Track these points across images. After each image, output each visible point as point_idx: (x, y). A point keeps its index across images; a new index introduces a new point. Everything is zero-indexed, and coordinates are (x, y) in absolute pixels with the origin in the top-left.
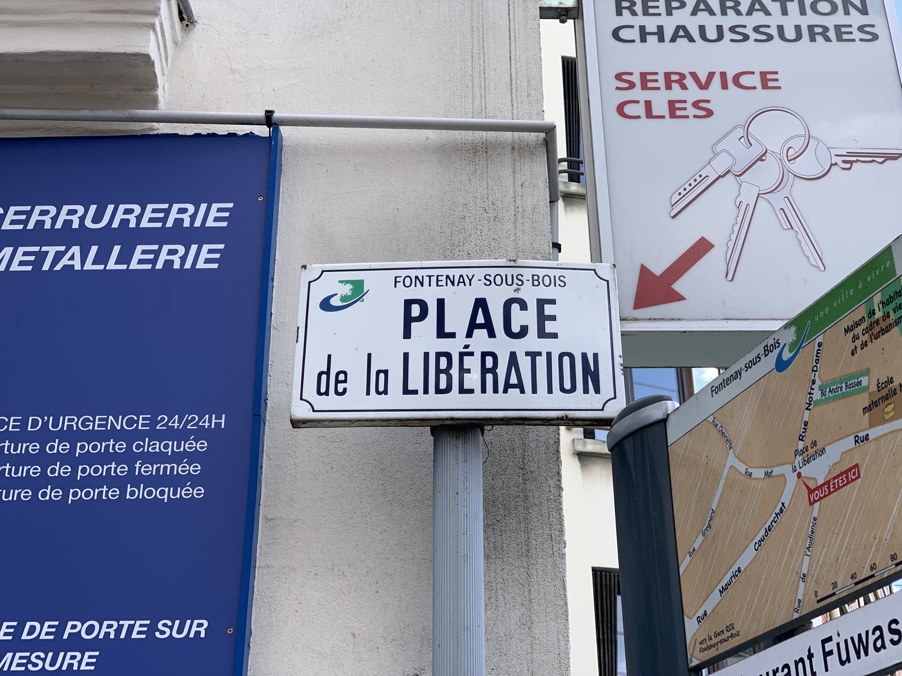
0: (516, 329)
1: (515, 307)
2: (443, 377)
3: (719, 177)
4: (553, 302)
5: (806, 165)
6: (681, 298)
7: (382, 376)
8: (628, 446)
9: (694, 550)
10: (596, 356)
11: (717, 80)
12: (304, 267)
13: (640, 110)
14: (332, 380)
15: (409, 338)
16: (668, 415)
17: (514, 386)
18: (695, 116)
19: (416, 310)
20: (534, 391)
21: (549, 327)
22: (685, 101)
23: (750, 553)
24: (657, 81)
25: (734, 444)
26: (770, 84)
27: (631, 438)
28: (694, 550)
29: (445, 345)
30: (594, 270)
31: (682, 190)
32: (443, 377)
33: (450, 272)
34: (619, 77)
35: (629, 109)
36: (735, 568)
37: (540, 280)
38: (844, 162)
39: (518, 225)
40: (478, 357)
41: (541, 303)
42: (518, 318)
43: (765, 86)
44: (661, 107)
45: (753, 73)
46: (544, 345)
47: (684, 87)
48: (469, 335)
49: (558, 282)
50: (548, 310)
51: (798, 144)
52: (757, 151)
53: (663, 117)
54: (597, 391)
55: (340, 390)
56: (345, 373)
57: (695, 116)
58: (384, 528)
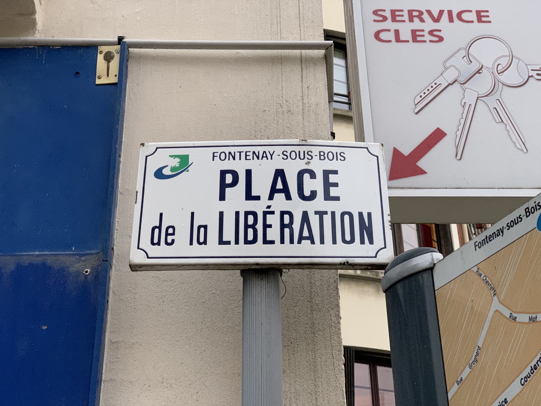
0: (307, 193)
1: (306, 176)
2: (250, 231)
3: (449, 85)
4: (335, 172)
5: (511, 77)
6: (423, 172)
7: (202, 230)
8: (399, 288)
9: (461, 379)
10: (369, 214)
11: (445, 16)
12: (143, 145)
13: (390, 36)
14: (163, 233)
15: (224, 200)
16: (434, 265)
17: (306, 238)
18: (431, 41)
19: (229, 179)
20: (322, 242)
21: (333, 192)
22: (423, 31)
23: (515, 388)
24: (403, 16)
25: (498, 292)
26: (484, 19)
27: (402, 283)
28: (461, 379)
29: (251, 205)
30: (367, 148)
31: (422, 94)
32: (250, 231)
33: (256, 149)
34: (375, 13)
35: (383, 36)
36: (501, 399)
37: (326, 156)
38: (538, 74)
39: (305, 118)
40: (277, 215)
41: (326, 173)
42: (309, 185)
43: (480, 20)
44: (406, 35)
45: (471, 11)
46: (329, 206)
47: (422, 21)
48: (271, 198)
49: (339, 157)
50: (332, 178)
51: (504, 62)
52: (475, 67)
53: (408, 41)
54: (371, 242)
55: (169, 241)
56: (173, 228)
57: (431, 41)
58: (203, 348)
